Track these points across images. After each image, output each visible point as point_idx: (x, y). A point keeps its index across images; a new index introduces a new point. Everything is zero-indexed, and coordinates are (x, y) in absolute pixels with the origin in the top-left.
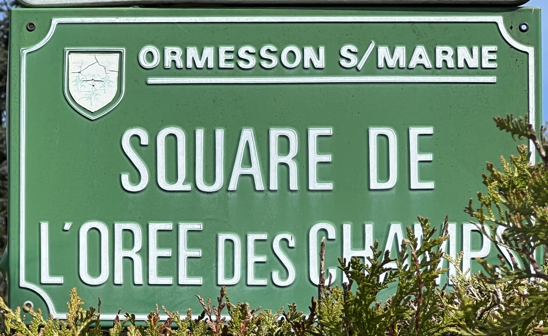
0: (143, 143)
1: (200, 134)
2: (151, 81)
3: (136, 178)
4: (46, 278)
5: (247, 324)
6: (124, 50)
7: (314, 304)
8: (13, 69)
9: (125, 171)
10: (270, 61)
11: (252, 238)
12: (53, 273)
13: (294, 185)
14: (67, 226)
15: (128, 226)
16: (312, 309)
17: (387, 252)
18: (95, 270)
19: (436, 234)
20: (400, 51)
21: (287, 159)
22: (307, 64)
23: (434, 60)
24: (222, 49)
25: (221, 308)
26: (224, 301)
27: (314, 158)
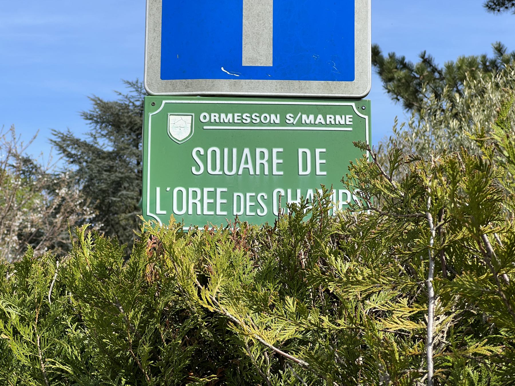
0: (201, 154)
1: (226, 150)
2: (205, 127)
3: (198, 168)
4: (159, 211)
5: (247, 230)
6: (193, 114)
7: (276, 222)
8: (145, 122)
9: (193, 166)
10: (256, 120)
11: (248, 195)
12: (161, 209)
13: (266, 173)
14: (168, 189)
15: (195, 189)
16: (276, 224)
17: (308, 199)
18: (180, 208)
19: (328, 191)
20: (312, 117)
21: (264, 161)
22: (272, 122)
23: (326, 121)
24: (236, 115)
25: (236, 223)
26: (237, 220)
27: (275, 161)
